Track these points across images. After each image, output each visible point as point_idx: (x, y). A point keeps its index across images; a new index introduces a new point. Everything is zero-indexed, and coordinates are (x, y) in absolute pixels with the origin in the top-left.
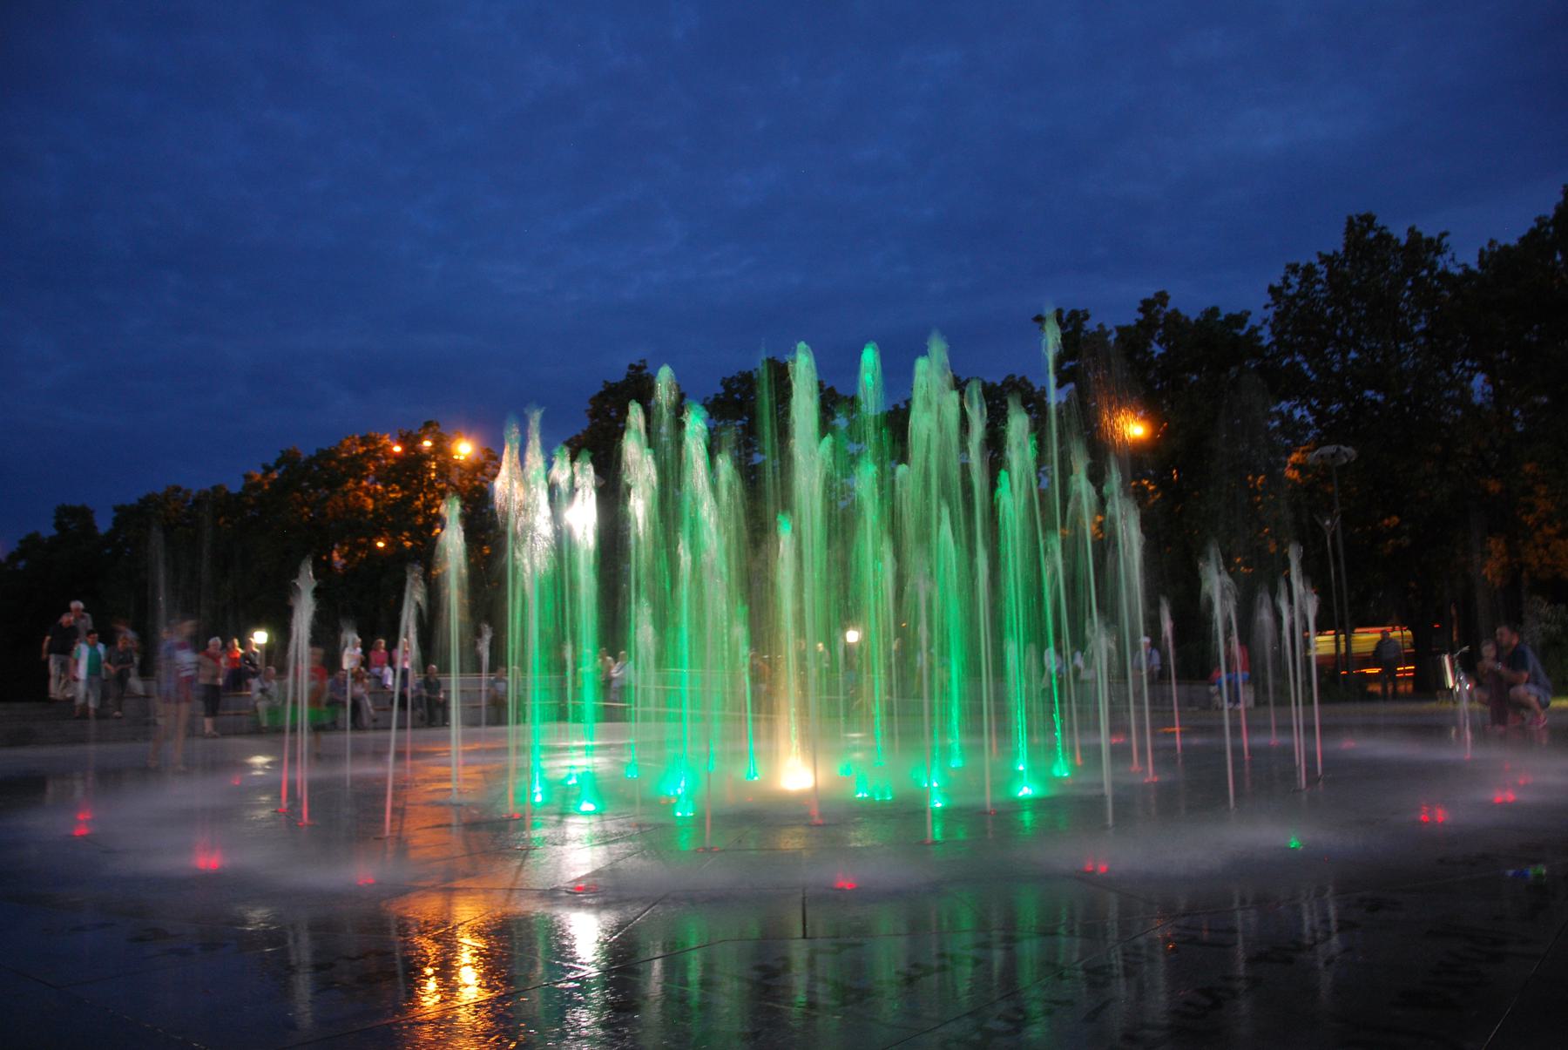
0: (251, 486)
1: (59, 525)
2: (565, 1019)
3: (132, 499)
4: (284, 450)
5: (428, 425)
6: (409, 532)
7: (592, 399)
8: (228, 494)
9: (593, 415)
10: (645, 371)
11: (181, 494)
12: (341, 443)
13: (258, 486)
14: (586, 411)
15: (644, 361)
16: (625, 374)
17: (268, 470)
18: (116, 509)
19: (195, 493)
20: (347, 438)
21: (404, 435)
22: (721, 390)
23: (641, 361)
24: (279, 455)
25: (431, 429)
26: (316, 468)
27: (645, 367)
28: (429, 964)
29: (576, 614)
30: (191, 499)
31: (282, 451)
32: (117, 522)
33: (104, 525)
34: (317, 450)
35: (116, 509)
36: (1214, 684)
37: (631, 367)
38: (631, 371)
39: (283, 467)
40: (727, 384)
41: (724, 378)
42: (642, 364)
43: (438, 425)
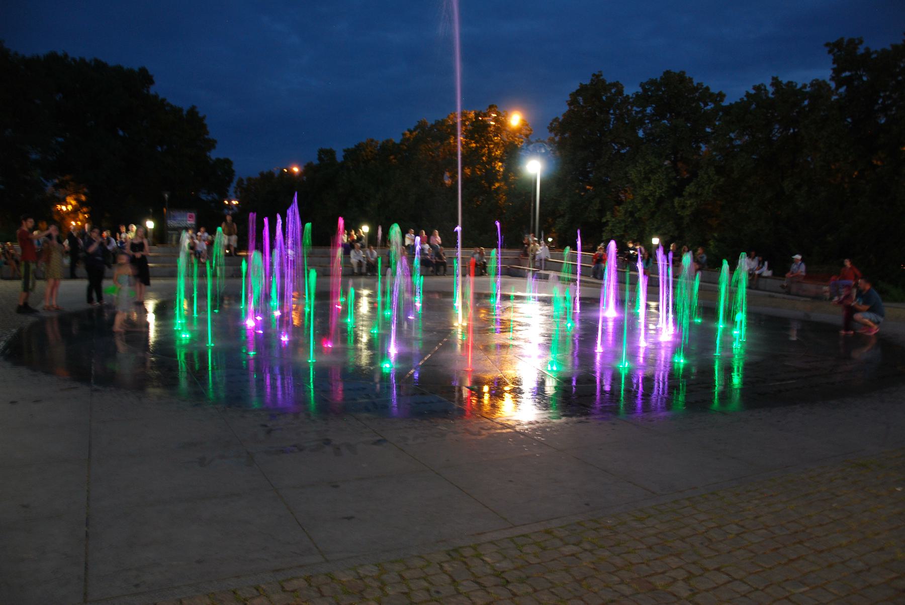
0: (736, 103)
1: (320, 159)
2: (643, 187)
3: (351, 146)
4: (419, 120)
5: (491, 107)
6: (806, 99)
7: (570, 95)
8: (394, 143)
9: (570, 104)
10: (601, 78)
11: (374, 143)
12: (448, 117)
13: (408, 139)
14: (567, 101)
15: (600, 72)
16: (590, 79)
17: (411, 132)
18: (345, 151)
19: (380, 142)
20: (452, 114)
21: (477, 113)
22: (640, 90)
23: (599, 72)
24: (417, 123)
25: (493, 109)
26: (435, 130)
27: (601, 75)
28: (440, 261)
29: (158, 278)
30: (379, 145)
31: (418, 122)
32: (345, 157)
33: (340, 157)
34: (436, 121)
35: (345, 151)
36: (662, 196)
37: (594, 75)
38: (593, 78)
39: (419, 130)
40: (152, 77)
41: (642, 83)
42: (600, 74)
43: (496, 107)
